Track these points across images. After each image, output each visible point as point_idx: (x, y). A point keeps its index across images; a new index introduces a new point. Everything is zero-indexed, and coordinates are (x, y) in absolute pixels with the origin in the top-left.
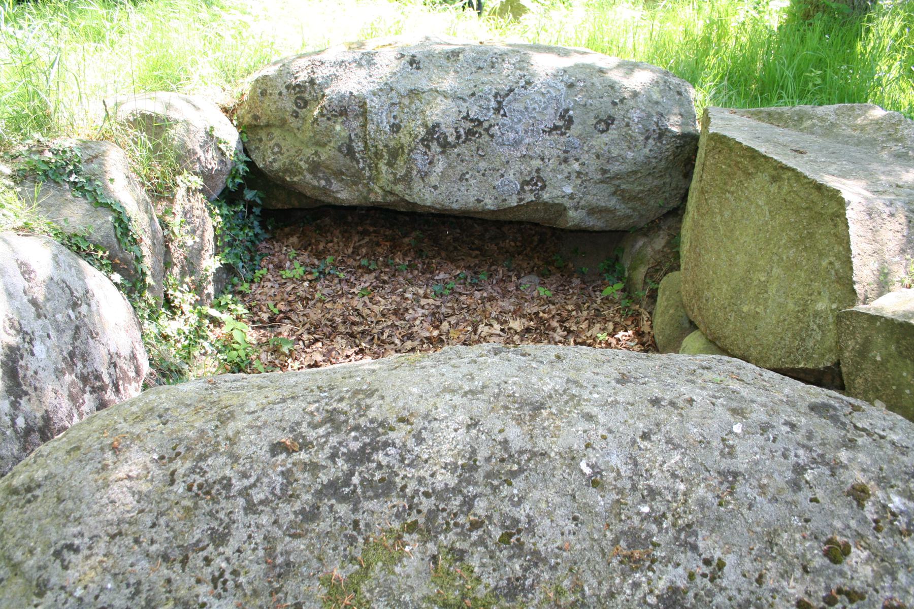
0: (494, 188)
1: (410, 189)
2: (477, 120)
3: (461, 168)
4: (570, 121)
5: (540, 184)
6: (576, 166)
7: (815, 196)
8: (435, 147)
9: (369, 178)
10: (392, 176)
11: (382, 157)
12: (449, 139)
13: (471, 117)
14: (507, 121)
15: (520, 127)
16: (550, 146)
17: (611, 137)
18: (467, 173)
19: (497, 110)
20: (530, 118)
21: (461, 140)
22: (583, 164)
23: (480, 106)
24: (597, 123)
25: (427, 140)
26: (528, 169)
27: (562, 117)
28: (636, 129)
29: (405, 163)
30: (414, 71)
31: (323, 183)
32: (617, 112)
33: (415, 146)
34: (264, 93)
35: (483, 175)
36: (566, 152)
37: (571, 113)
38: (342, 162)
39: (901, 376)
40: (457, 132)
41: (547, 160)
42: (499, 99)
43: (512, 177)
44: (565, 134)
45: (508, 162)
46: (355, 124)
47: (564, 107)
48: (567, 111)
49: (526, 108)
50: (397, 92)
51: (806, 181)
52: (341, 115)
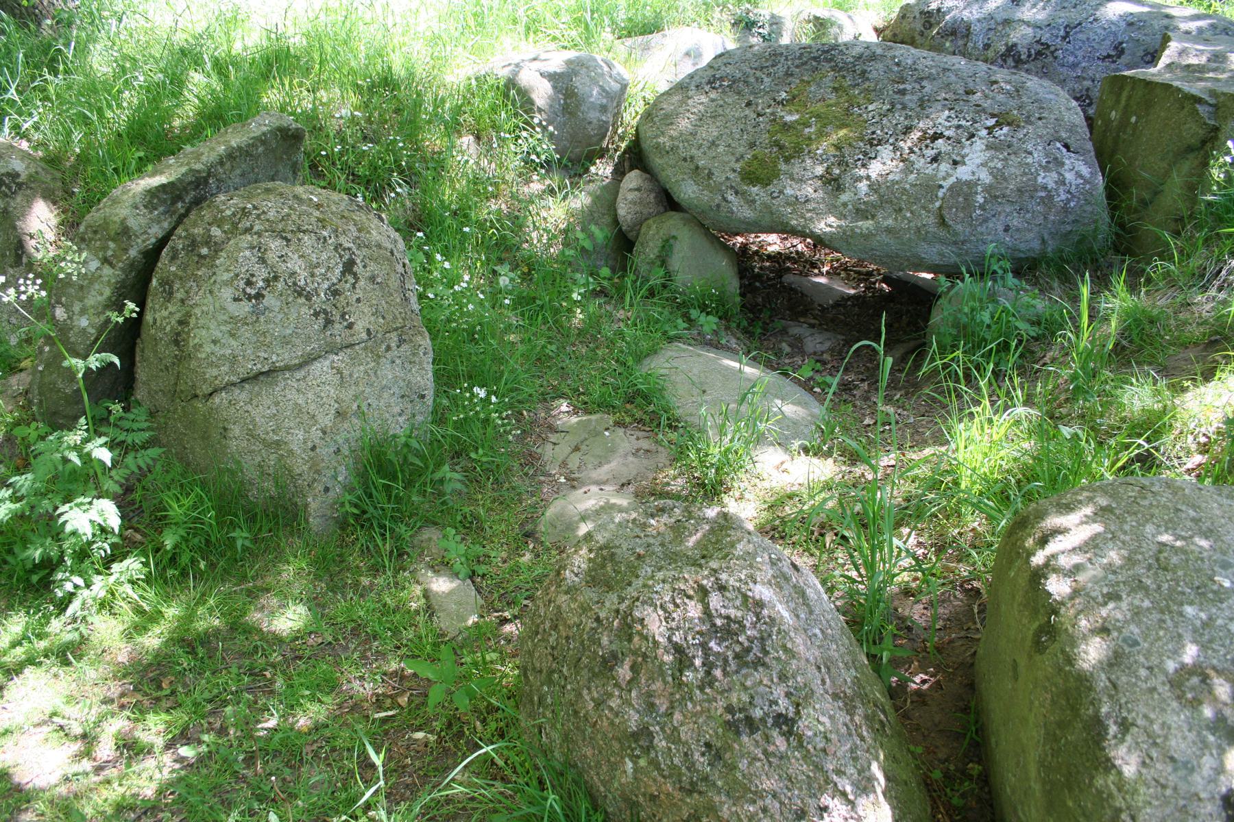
14: (1070, 47)
15: (1080, 54)
19: (1064, 38)
27: (1116, 48)
34: (904, 17)
48: (1121, 43)
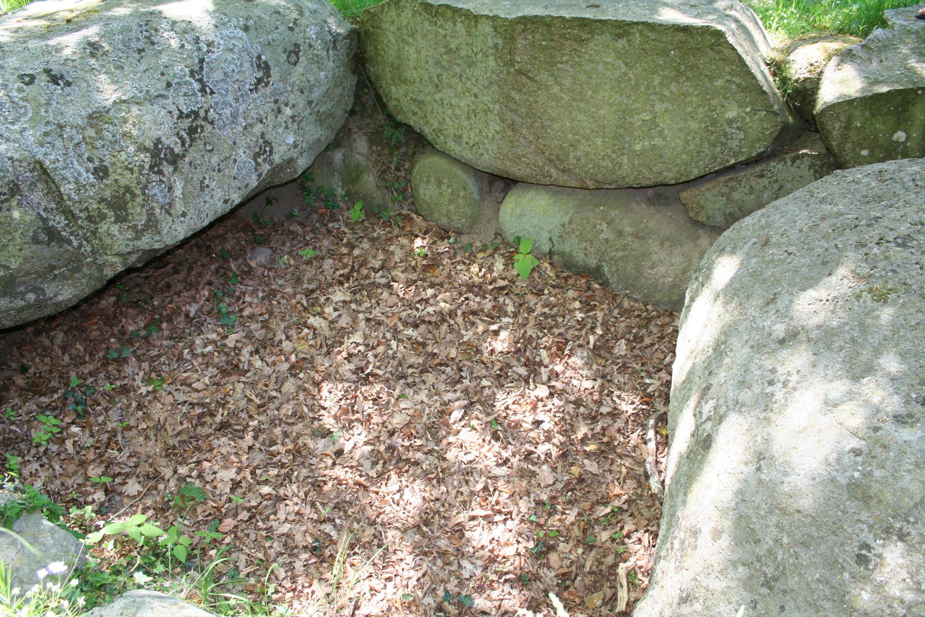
0: (235, 178)
1: (159, 233)
2: (193, 112)
3: (197, 177)
4: (266, 68)
5: (267, 149)
6: (288, 111)
7: (681, 36)
8: (167, 169)
9: (93, 252)
10: (130, 232)
12: (176, 151)
13: (185, 111)
16: (259, 103)
17: (303, 65)
18: (204, 178)
19: (203, 90)
20: (234, 83)
21: (187, 145)
22: (294, 106)
23: (185, 95)
24: (288, 57)
25: (156, 165)
26: (254, 139)
28: (318, 45)
29: (143, 206)
30: (67, 90)
31: (31, 297)
32: (297, 37)
33: (147, 180)
35: (219, 171)
36: (276, 102)
37: (263, 57)
38: (47, 255)
39: (876, 128)
40: (180, 138)
41: (265, 121)
42: (197, 77)
43: (243, 155)
44: (269, 82)
45: (235, 143)
46: (37, 196)
47: (255, 55)
48: (259, 58)
49: (226, 74)
51: (663, 28)
52: (13, 196)
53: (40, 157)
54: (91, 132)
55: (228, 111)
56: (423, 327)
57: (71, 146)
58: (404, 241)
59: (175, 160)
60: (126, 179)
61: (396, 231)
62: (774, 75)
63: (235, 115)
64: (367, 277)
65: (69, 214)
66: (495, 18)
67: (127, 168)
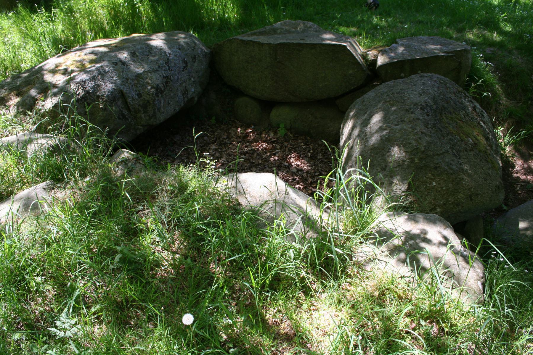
11: (139, 111)
12: (162, 89)
19: (169, 69)
36: (189, 75)
43: (179, 94)
50: (131, 79)
53: (122, 89)
54: (136, 82)
55: (176, 77)
56: (247, 155)
57: (130, 86)
58: (234, 129)
59: (162, 92)
60: (148, 98)
61: (230, 126)
62: (363, 59)
63: (178, 78)
64: (222, 141)
65: (128, 109)
66: (270, 44)
67: (148, 94)
